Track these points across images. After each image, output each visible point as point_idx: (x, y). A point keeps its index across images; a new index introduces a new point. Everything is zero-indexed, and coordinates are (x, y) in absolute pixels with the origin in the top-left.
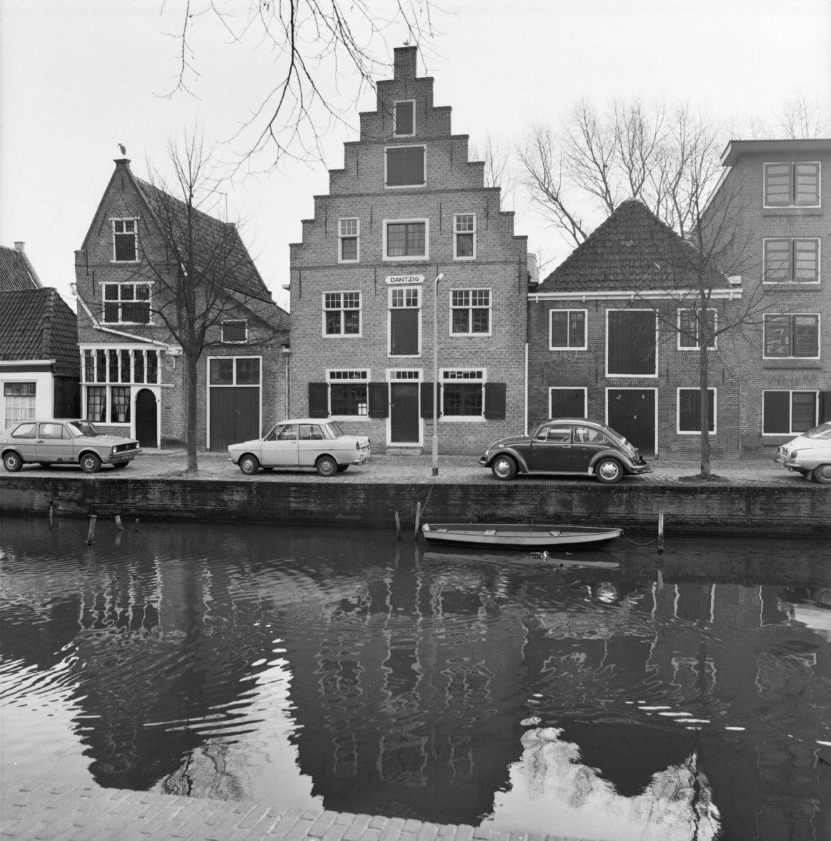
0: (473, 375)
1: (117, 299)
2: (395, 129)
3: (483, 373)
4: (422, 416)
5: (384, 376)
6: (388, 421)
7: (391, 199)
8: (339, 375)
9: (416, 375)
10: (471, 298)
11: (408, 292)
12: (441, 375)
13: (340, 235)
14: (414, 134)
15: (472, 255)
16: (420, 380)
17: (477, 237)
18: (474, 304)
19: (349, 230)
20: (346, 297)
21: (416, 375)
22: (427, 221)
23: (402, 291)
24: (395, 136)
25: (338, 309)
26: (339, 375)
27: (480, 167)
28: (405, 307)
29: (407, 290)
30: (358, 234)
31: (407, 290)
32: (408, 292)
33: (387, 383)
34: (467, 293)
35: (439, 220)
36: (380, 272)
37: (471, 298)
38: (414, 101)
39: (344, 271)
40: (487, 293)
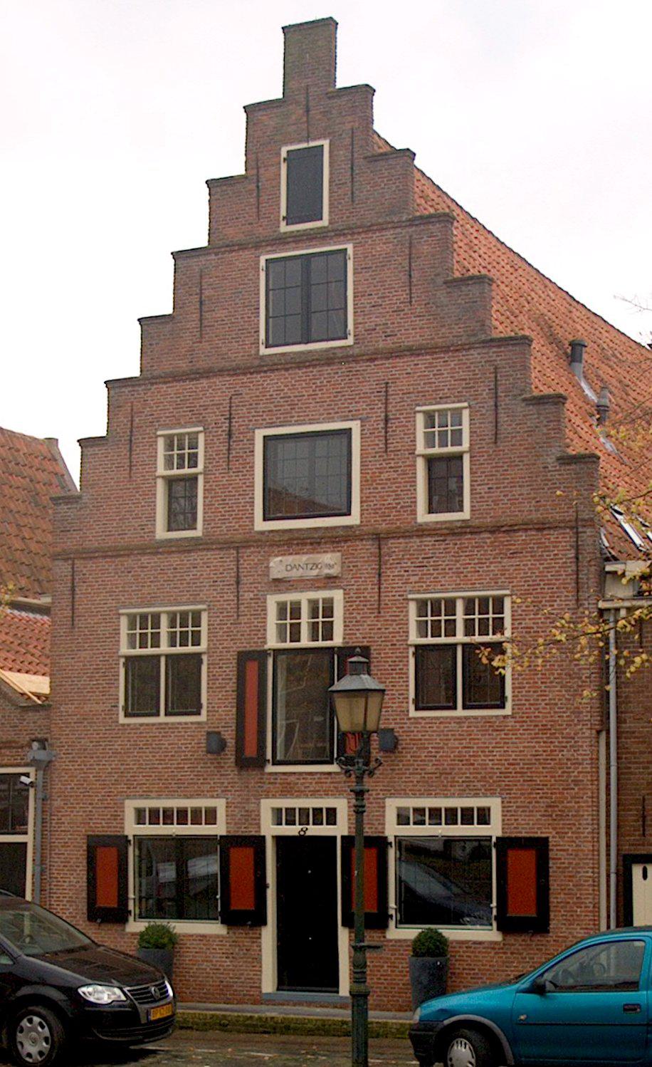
0: (467, 815)
1: (318, 618)
2: (283, 212)
3: (400, 805)
4: (343, 925)
5: (118, 817)
6: (268, 936)
7: (273, 383)
8: (154, 816)
9: (332, 816)
10: (460, 617)
11: (314, 605)
12: (130, 816)
13: (421, 448)
14: (325, 222)
15: (461, 510)
16: (341, 829)
17: (206, 482)
18: (469, 631)
19: (443, 435)
20: (469, 610)
21: (484, 817)
22: (355, 426)
23: (299, 603)
24: (284, 228)
25: (450, 640)
26: (154, 816)
27: (475, 290)
28: (305, 642)
29: (310, 601)
30: (466, 445)
31: (310, 601)
32: (314, 605)
33: (264, 837)
34: (451, 605)
35: (382, 425)
36: (250, 558)
37: (460, 617)
38: (326, 143)
39: (175, 559)
40: (499, 603)
